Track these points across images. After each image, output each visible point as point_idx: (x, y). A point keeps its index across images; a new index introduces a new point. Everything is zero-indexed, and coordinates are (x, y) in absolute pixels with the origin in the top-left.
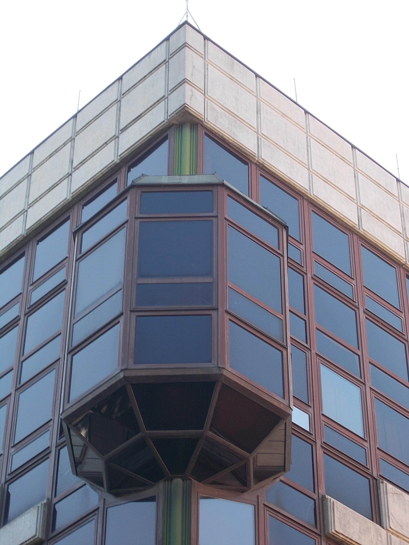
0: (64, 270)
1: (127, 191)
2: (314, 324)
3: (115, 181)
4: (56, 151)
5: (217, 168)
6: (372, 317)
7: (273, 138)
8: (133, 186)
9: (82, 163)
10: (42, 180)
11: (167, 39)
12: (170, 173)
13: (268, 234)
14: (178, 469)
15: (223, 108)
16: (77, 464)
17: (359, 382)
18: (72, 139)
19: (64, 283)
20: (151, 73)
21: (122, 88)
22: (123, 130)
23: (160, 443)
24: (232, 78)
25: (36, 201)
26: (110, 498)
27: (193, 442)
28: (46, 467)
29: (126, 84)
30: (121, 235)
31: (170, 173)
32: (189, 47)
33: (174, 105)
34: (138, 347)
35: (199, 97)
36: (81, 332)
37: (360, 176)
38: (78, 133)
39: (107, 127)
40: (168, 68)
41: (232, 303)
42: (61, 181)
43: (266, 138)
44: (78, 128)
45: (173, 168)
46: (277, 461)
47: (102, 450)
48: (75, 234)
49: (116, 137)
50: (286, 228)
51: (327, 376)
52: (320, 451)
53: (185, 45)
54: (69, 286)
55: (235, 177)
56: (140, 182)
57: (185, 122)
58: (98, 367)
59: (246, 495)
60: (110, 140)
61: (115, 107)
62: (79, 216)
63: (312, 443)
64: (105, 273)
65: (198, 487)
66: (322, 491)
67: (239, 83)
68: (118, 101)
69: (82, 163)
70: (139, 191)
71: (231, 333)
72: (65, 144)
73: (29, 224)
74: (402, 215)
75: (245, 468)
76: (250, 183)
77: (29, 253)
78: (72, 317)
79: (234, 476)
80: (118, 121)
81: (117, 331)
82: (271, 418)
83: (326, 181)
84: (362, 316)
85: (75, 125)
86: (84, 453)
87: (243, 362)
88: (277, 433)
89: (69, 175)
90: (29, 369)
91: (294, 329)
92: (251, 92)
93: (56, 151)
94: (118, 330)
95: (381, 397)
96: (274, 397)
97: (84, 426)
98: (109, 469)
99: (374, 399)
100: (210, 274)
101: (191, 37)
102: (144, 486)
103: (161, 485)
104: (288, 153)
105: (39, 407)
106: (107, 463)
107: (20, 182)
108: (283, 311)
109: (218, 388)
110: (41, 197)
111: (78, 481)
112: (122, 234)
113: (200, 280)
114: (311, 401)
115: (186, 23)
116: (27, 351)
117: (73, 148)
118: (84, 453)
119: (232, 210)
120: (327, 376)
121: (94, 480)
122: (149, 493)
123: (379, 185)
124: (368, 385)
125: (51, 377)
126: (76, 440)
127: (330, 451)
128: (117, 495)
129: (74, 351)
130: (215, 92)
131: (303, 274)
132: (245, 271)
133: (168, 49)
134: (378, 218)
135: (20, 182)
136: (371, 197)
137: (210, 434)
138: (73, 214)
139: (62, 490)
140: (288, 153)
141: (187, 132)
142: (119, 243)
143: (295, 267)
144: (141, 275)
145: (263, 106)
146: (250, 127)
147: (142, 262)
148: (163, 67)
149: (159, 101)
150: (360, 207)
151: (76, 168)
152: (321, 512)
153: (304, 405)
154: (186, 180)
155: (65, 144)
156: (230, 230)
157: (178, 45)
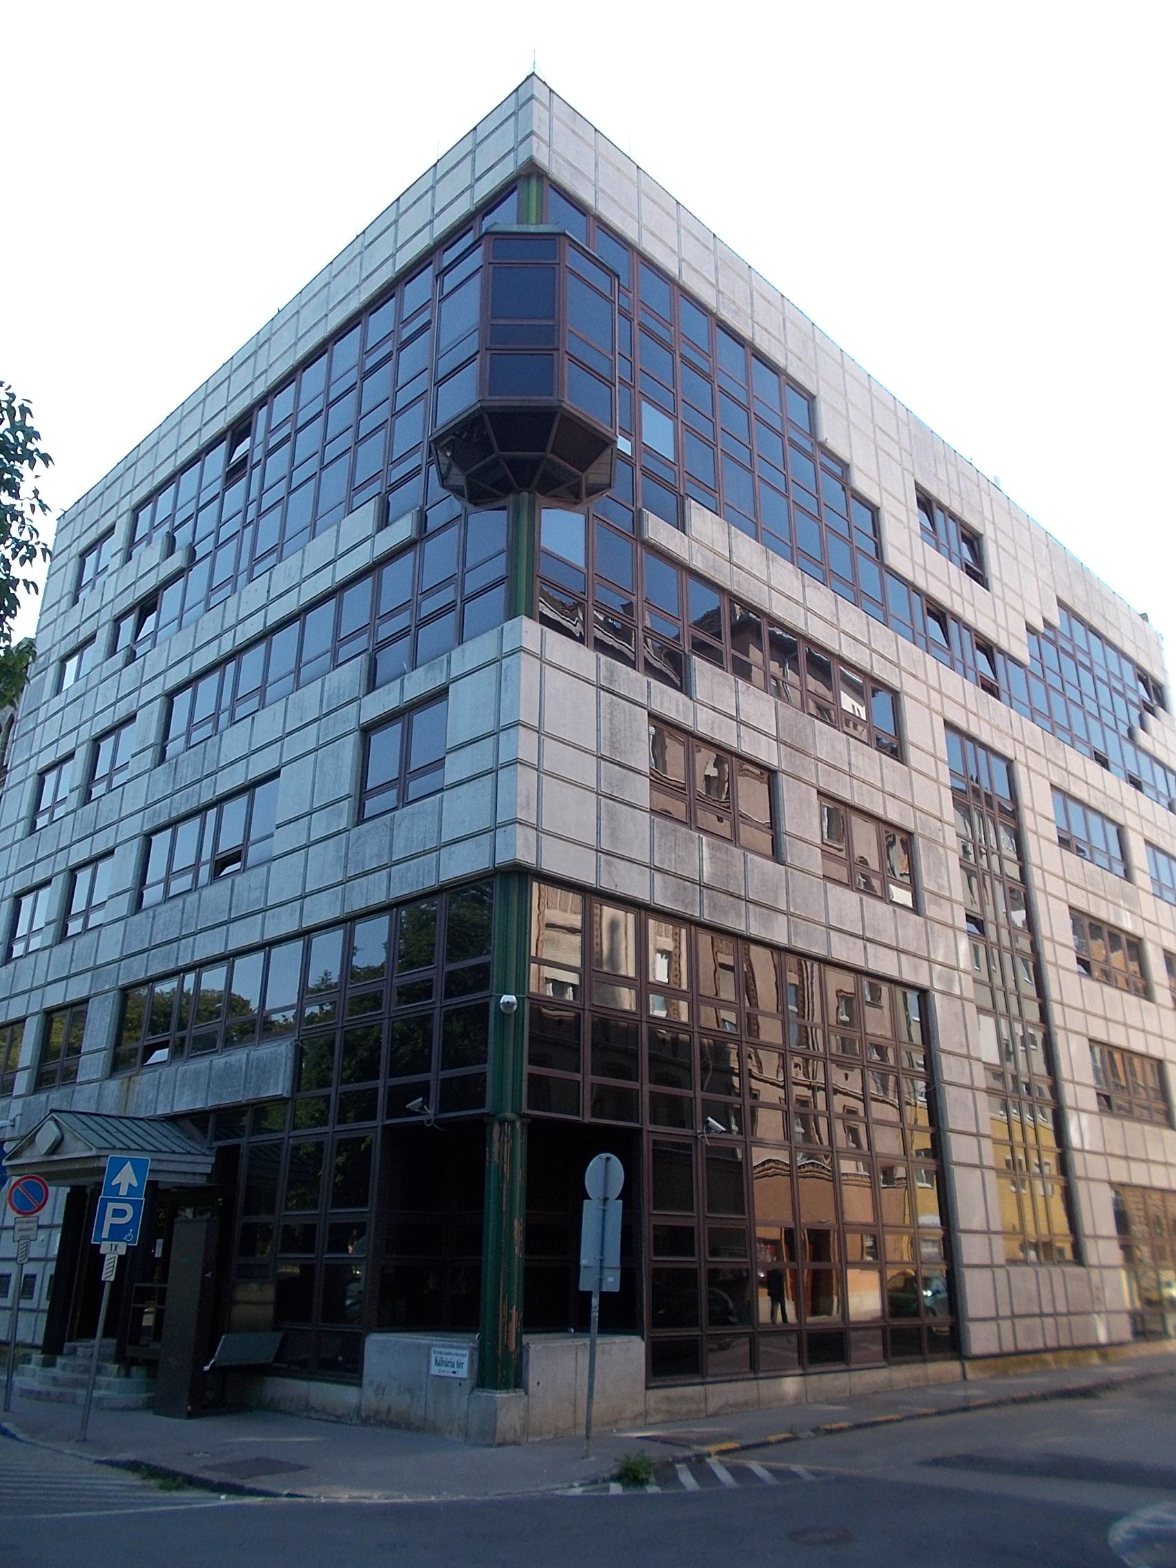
0: (428, 311)
1: (481, 238)
2: (638, 366)
3: (431, 263)
4: (419, 199)
5: (559, 220)
6: (686, 361)
7: (609, 192)
8: (486, 233)
9: (442, 211)
10: (409, 225)
11: (516, 90)
12: (519, 222)
13: (602, 281)
14: (525, 484)
15: (566, 161)
16: (443, 479)
17: (673, 416)
18: (433, 187)
19: (429, 322)
20: (502, 124)
21: (476, 138)
22: (478, 180)
23: (512, 463)
24: (574, 132)
25: (403, 245)
26: (471, 507)
27: (536, 463)
28: (419, 480)
29: (480, 135)
30: (477, 280)
31: (519, 222)
32: (536, 99)
33: (523, 158)
34: (491, 382)
35: (545, 149)
36: (445, 367)
37: (682, 231)
38: (438, 182)
39: (463, 176)
40: (517, 119)
41: (570, 344)
42: (424, 227)
43: (603, 191)
44: (438, 177)
45: (522, 218)
46: (605, 480)
47: (463, 468)
48: (437, 277)
49: (471, 187)
50: (618, 276)
51: (647, 410)
52: (639, 473)
53: (532, 97)
54: (434, 325)
55: (576, 229)
56: (493, 229)
57: (531, 173)
58: (459, 398)
59: (579, 507)
60: (467, 189)
61: (470, 157)
62: (441, 260)
63: (633, 466)
64: (463, 313)
65: (541, 499)
66: (639, 505)
67: (580, 137)
68: (472, 151)
69: (442, 211)
70: (492, 238)
71: (568, 371)
72: (427, 192)
73: (155, 483)
74: (716, 268)
75: (579, 484)
76: (588, 233)
77: (398, 295)
78: (437, 354)
79: (571, 493)
80: (473, 171)
81: (474, 367)
82: (601, 444)
83: (653, 234)
84: (678, 359)
85: (435, 174)
86: (449, 470)
87: (579, 398)
88: (605, 457)
89: (431, 222)
90: (403, 399)
91: (621, 370)
92: (590, 146)
93: (419, 199)
94: (475, 365)
95: (688, 429)
96: (605, 428)
97: (448, 449)
98: (469, 483)
99: (685, 431)
100: (552, 317)
101: (540, 91)
102: (499, 497)
103: (511, 497)
104: (621, 207)
105: (412, 431)
106: (467, 477)
107: (389, 227)
108: (613, 354)
109: (558, 418)
110: (407, 242)
111: (445, 493)
112: (478, 277)
113: (544, 322)
114: (632, 432)
115: (533, 74)
116: (363, 412)
117: (434, 195)
118: (449, 470)
119: (572, 259)
120: (647, 410)
121: (458, 492)
122: (502, 503)
123: (698, 239)
124: (680, 418)
125: (420, 406)
126: (443, 460)
127: (646, 473)
128: (476, 505)
129: (439, 383)
130: (558, 145)
131: (631, 321)
132: (583, 317)
133: (517, 99)
134: (696, 271)
135: (389, 227)
136: (691, 251)
137: (552, 456)
138: (476, 223)
139: (432, 499)
140: (621, 207)
141: (534, 183)
142: (475, 284)
143: (625, 314)
144: (493, 317)
145: (600, 160)
146: (589, 180)
147: (494, 304)
148: (513, 118)
149: (509, 152)
150: (681, 260)
151: (437, 215)
152: (637, 522)
153: (627, 435)
154: (532, 229)
155: (427, 192)
156: (570, 277)
157: (527, 96)
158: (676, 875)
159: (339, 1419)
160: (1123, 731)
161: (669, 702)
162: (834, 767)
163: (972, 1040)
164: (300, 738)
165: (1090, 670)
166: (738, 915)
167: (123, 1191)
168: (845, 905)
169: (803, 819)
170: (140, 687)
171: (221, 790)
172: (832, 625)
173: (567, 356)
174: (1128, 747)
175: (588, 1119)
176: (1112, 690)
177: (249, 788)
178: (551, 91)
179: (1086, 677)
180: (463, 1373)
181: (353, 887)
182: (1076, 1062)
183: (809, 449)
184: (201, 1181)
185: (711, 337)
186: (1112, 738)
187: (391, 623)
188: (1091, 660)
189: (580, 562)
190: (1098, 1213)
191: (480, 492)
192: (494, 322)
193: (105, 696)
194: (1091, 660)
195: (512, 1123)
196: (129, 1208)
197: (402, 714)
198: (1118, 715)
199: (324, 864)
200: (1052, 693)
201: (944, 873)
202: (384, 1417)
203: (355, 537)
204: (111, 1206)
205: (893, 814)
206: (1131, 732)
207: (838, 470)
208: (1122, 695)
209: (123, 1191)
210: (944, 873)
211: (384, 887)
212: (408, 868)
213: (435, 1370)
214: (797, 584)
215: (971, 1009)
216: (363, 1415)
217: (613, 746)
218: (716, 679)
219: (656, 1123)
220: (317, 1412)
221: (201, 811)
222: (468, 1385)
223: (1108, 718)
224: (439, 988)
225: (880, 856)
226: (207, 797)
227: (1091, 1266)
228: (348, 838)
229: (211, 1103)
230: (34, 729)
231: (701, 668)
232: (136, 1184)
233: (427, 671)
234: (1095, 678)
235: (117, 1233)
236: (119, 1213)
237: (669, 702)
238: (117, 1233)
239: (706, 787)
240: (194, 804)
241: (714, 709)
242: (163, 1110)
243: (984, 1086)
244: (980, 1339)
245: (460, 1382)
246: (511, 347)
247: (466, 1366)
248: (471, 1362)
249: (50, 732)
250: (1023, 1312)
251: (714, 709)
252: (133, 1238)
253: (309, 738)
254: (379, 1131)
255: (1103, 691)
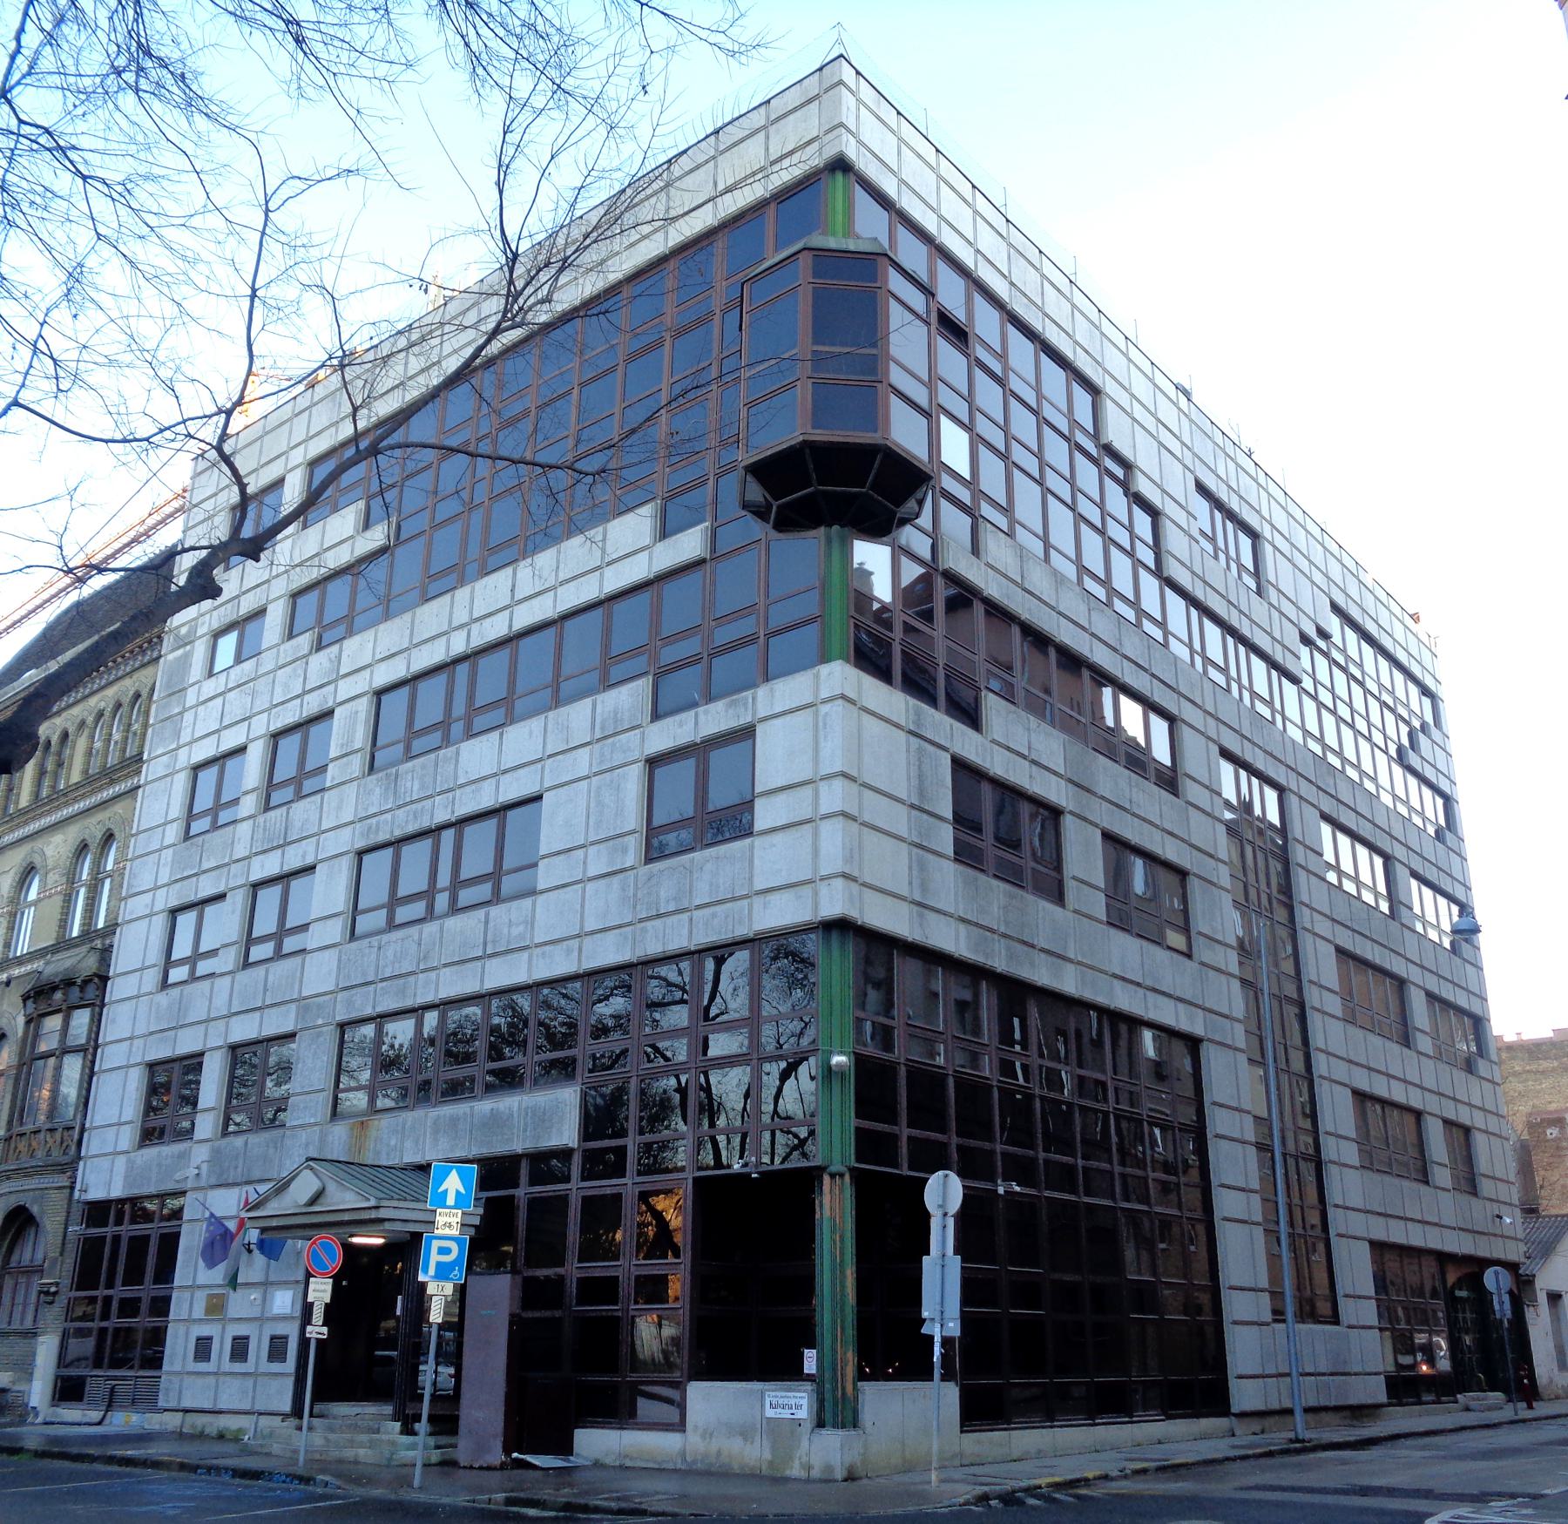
5: (870, 226)
26: (774, 534)
158: (977, 925)
160: (1393, 750)
161: (968, 744)
162: (1117, 806)
163: (1234, 1088)
164: (578, 765)
165: (1361, 684)
166: (1032, 965)
168: (1124, 951)
169: (1083, 857)
170: (336, 680)
171: (463, 810)
172: (1115, 650)
174: (1398, 771)
175: (906, 1172)
176: (1384, 704)
177: (498, 812)
178: (858, 73)
179: (1357, 691)
180: (803, 1414)
181: (644, 930)
182: (1337, 1113)
183: (1094, 451)
185: (932, 273)
186: (1381, 759)
187: (662, 643)
188: (1363, 672)
189: (1168, 763)
190: (1355, 1271)
191: (790, 520)
193: (286, 685)
194: (1363, 672)
195: (842, 1175)
196: (454, 1247)
197: (699, 751)
198: (1388, 732)
199: (602, 903)
200: (1324, 712)
201: (1220, 917)
203: (628, 547)
204: (436, 1244)
205: (1170, 851)
206: (1400, 749)
207: (1119, 472)
208: (1344, 670)
210: (1220, 917)
211: (685, 932)
212: (714, 915)
213: (770, 1413)
214: (1083, 608)
215: (1242, 1058)
217: (922, 793)
218: (1011, 716)
221: (433, 832)
222: (808, 1426)
223: (1378, 738)
225: (1151, 894)
226: (442, 816)
228: (636, 877)
230: (181, 713)
231: (993, 707)
233: (730, 705)
234: (1367, 691)
235: (443, 1272)
236: (443, 1251)
237: (968, 744)
238: (443, 1272)
239: (999, 828)
240: (425, 823)
241: (1008, 749)
243: (1253, 1140)
244: (1244, 1396)
247: (805, 1407)
248: (810, 1406)
249: (208, 719)
251: (1008, 749)
252: (459, 1275)
253: (582, 762)
254: (690, 1181)
255: (1374, 705)
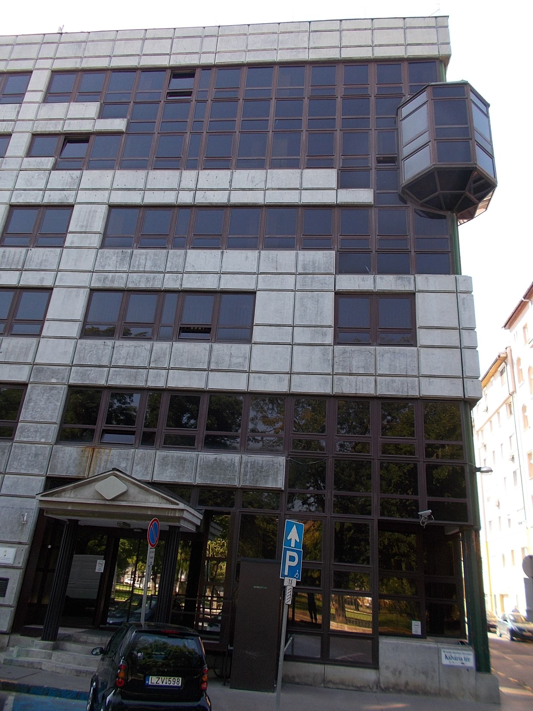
100: (467, 124)
159: (359, 689)
167: (293, 545)
173: (476, 143)
184: (193, 529)
192: (437, 127)
196: (295, 555)
202: (403, 688)
204: (289, 553)
209: (293, 545)
213: (445, 662)
216: (382, 686)
219: (432, 496)
220: (334, 683)
224: (67, 307)
227: (13, 131)
229: (199, 481)
232: (298, 541)
242: (148, 478)
245: (468, 669)
246: (445, 138)
250: (432, 29)
